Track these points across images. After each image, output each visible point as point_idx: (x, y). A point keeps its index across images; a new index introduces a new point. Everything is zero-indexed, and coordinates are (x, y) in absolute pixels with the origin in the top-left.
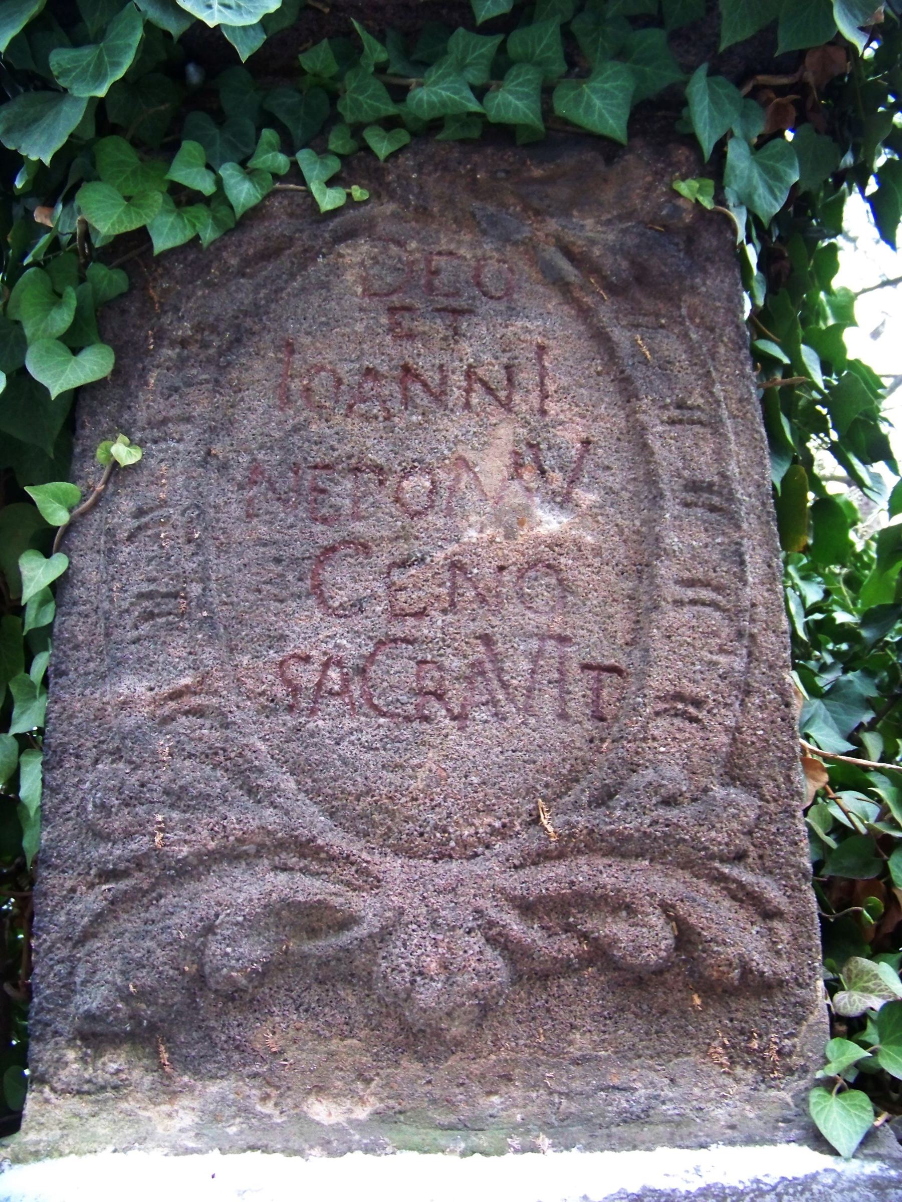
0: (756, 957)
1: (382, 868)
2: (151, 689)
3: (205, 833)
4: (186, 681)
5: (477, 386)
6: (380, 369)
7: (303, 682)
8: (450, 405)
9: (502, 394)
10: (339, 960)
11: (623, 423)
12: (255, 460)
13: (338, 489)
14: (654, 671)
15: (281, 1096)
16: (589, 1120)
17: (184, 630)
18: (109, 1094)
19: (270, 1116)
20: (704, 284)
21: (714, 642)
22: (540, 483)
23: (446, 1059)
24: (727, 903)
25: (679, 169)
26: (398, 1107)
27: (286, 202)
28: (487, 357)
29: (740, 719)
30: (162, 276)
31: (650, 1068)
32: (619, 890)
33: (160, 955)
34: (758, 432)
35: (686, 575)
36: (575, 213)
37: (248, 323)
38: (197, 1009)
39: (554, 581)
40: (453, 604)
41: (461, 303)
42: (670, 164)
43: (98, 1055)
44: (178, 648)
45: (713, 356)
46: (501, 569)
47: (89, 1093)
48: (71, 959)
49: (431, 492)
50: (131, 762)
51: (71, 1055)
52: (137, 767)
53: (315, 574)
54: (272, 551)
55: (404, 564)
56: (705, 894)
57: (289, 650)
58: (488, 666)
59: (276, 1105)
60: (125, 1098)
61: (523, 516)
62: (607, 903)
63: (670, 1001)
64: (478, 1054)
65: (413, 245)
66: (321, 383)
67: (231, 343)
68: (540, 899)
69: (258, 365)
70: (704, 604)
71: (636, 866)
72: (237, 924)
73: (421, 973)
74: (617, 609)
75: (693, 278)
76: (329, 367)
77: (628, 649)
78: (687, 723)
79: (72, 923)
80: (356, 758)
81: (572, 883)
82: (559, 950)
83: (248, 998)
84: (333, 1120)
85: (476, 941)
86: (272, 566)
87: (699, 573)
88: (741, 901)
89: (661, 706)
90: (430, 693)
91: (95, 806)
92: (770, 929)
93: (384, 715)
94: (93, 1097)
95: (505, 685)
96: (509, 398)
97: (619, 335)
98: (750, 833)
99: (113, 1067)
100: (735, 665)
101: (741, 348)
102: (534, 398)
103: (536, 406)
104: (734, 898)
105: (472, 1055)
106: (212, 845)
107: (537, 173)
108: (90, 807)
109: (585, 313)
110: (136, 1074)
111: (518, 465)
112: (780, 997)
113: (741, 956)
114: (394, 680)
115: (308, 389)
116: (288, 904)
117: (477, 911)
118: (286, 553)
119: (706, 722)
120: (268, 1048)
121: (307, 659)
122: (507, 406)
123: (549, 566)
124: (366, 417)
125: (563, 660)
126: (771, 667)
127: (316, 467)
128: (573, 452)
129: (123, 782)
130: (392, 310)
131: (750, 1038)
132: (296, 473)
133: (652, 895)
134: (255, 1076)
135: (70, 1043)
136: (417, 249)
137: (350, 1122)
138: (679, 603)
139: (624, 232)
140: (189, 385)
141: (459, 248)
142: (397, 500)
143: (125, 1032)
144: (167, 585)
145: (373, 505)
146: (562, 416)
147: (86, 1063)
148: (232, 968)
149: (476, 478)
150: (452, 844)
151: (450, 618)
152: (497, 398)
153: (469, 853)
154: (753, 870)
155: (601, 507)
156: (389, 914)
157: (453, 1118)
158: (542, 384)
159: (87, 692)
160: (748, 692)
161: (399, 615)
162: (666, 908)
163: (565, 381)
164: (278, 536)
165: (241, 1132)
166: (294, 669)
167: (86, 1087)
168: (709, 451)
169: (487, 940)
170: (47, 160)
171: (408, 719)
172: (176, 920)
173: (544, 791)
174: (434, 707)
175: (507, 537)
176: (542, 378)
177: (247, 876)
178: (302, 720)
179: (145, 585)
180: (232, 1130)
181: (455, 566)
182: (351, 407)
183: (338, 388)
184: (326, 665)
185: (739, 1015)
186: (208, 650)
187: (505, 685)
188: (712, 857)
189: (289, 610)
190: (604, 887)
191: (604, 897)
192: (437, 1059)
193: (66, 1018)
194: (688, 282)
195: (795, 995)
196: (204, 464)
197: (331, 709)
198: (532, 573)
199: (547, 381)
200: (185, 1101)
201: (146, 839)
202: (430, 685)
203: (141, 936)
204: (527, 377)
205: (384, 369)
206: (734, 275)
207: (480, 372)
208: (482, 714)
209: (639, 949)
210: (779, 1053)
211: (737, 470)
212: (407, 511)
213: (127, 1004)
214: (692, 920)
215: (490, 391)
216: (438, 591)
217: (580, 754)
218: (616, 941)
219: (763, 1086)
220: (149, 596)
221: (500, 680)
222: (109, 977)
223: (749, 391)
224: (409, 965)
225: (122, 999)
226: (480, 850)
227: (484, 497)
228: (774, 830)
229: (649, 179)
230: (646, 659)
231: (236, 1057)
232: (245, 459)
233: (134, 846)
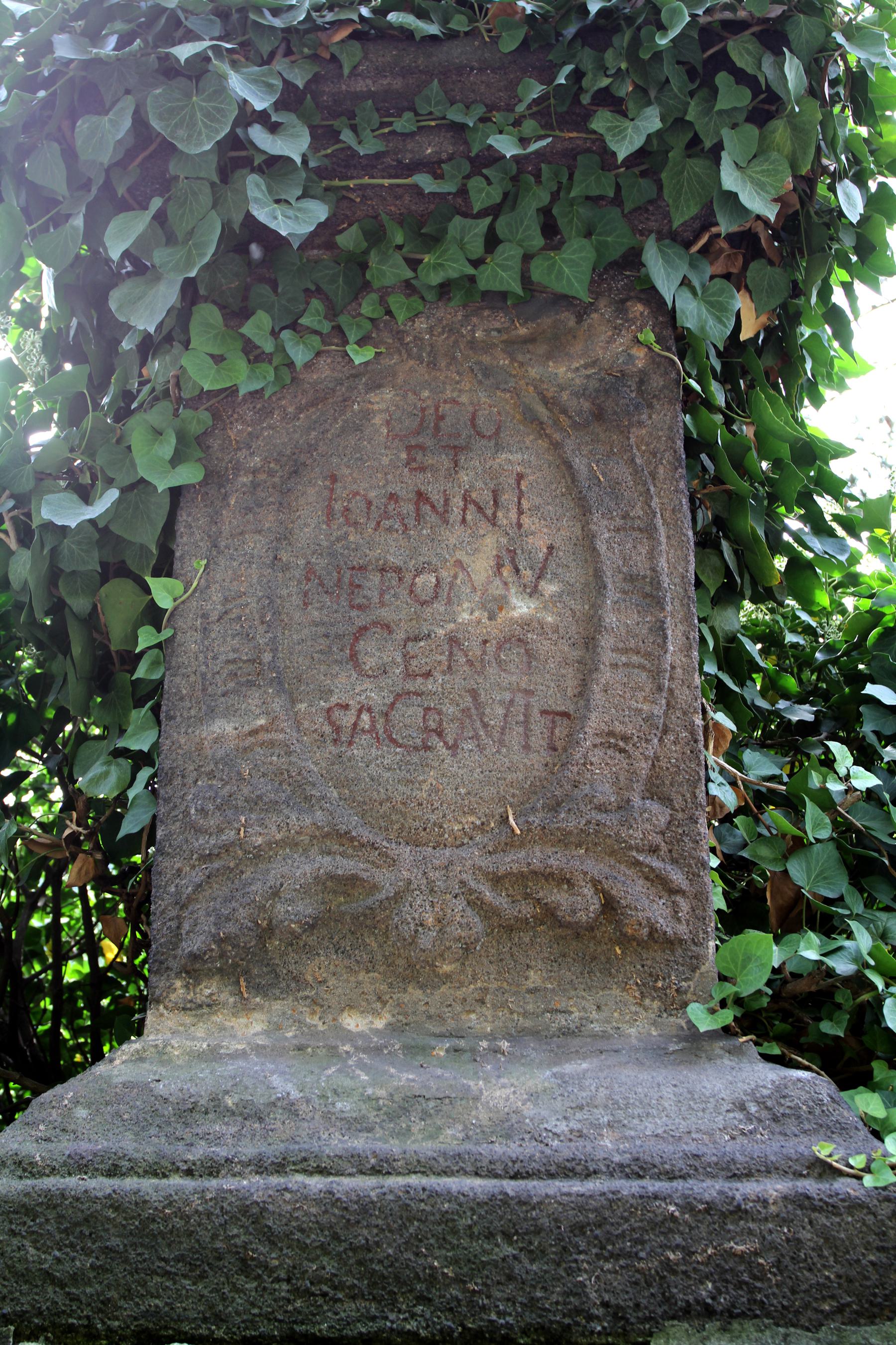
0: (661, 921)
1: (397, 852)
2: (236, 729)
3: (274, 828)
4: (262, 722)
5: (471, 507)
6: (399, 493)
7: (344, 723)
8: (451, 521)
9: (489, 512)
10: (365, 915)
11: (580, 532)
12: (309, 563)
13: (368, 584)
14: (593, 716)
15: (324, 1012)
16: (538, 1032)
17: (259, 686)
18: (205, 1010)
19: (315, 1026)
20: (650, 418)
21: (640, 695)
22: (516, 579)
23: (439, 987)
24: (641, 882)
25: (634, 323)
26: (404, 1021)
27: (329, 361)
28: (479, 484)
29: (659, 750)
30: (237, 421)
31: (583, 998)
32: (562, 870)
33: (242, 913)
34: (685, 535)
35: (621, 645)
36: (551, 364)
37: (303, 458)
38: (266, 951)
39: (523, 651)
40: (450, 667)
41: (462, 442)
42: (627, 321)
43: (198, 982)
44: (254, 699)
45: (653, 475)
46: (485, 642)
47: (190, 1009)
48: (178, 917)
49: (436, 586)
50: (222, 780)
51: (178, 983)
52: (227, 783)
53: (352, 646)
54: (322, 630)
55: (417, 639)
56: (624, 875)
57: (334, 700)
58: (473, 711)
59: (320, 1018)
60: (215, 1013)
61: (502, 603)
62: (554, 879)
63: (599, 950)
64: (462, 984)
65: (426, 394)
66: (357, 505)
67: (291, 474)
68: (508, 875)
69: (311, 491)
70: (634, 667)
71: (574, 853)
72: (295, 890)
73: (422, 925)
74: (569, 672)
75: (640, 414)
76: (362, 492)
77: (575, 699)
78: (617, 753)
79: (178, 893)
80: (380, 776)
81: (529, 864)
82: (520, 912)
83: (301, 943)
84: (360, 1028)
85: (460, 904)
86: (321, 641)
87: (632, 644)
88: (653, 881)
89: (598, 740)
90: (433, 730)
91: (196, 810)
92: (673, 902)
93: (400, 747)
94: (194, 1012)
95: (485, 725)
96: (494, 514)
97: (579, 463)
98: (663, 833)
99: (208, 992)
100: (656, 712)
101: (676, 469)
102: (513, 515)
103: (514, 521)
104: (647, 878)
105: (457, 985)
106: (278, 837)
107: (523, 331)
108: (193, 811)
109: (556, 446)
110: (224, 997)
111: (499, 566)
112: (679, 952)
113: (648, 919)
114: (408, 721)
115: (347, 509)
116: (332, 877)
117: (461, 882)
118: (333, 631)
119: (631, 752)
120: (315, 978)
121: (346, 707)
122: (493, 521)
123: (519, 640)
124: (390, 530)
125: (527, 706)
126: (685, 713)
127: (353, 568)
128: (541, 555)
129: (217, 793)
130: (409, 448)
131: (656, 981)
132: (339, 573)
133: (586, 874)
134: (307, 997)
135: (178, 975)
136: (429, 397)
137: (371, 1029)
138: (614, 666)
139: (588, 377)
140: (260, 506)
141: (459, 396)
142: (411, 592)
143: (217, 968)
144: (247, 654)
145: (394, 596)
146: (533, 528)
147: (188, 989)
148: (291, 921)
149: (469, 575)
150: (446, 836)
151: (447, 678)
152: (485, 516)
153: (458, 843)
154: (663, 860)
155: (560, 596)
156: (401, 884)
157: (443, 1029)
158: (519, 503)
159: (190, 731)
160: (665, 731)
161: (409, 675)
162: (595, 883)
163: (538, 501)
164: (326, 619)
165: (295, 1036)
166: (337, 714)
167: (189, 1006)
168: (644, 551)
169: (468, 903)
170: (152, 330)
171: (416, 748)
172: (253, 888)
173: (512, 800)
174: (434, 740)
175: (490, 619)
176: (519, 499)
177: (303, 859)
178: (343, 749)
179: (231, 654)
180: (289, 1035)
181: (453, 640)
182: (378, 523)
183: (369, 508)
184: (360, 712)
185: (649, 963)
186: (276, 700)
187: (485, 725)
188: (631, 848)
189: (334, 672)
190: (551, 867)
191: (552, 874)
192: (434, 988)
193: (175, 957)
194: (636, 418)
195: (691, 951)
196: (272, 566)
197: (363, 742)
198: (508, 646)
199: (523, 501)
200: (257, 1015)
201: (233, 833)
202: (432, 725)
203: (227, 900)
204: (508, 497)
205: (402, 494)
206: (675, 409)
207: (474, 495)
208: (469, 745)
209: (574, 912)
210: (677, 991)
211: (665, 565)
212: (417, 601)
213: (219, 946)
214: (614, 892)
215: (480, 509)
216: (439, 658)
217: (538, 774)
218: (559, 905)
219: (665, 1015)
220: (234, 661)
221: (482, 721)
222: (206, 928)
223: (681, 502)
224: (414, 919)
225: (215, 942)
226: (466, 841)
227: (474, 589)
228: (680, 831)
229: (610, 333)
230: (587, 707)
231: (293, 985)
232: (301, 562)
233: (224, 838)
